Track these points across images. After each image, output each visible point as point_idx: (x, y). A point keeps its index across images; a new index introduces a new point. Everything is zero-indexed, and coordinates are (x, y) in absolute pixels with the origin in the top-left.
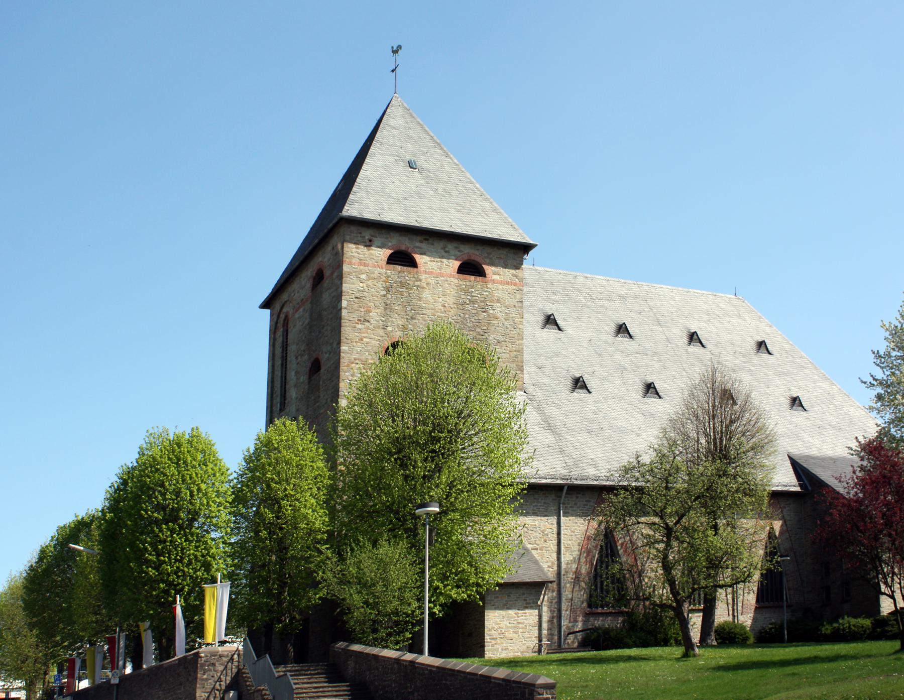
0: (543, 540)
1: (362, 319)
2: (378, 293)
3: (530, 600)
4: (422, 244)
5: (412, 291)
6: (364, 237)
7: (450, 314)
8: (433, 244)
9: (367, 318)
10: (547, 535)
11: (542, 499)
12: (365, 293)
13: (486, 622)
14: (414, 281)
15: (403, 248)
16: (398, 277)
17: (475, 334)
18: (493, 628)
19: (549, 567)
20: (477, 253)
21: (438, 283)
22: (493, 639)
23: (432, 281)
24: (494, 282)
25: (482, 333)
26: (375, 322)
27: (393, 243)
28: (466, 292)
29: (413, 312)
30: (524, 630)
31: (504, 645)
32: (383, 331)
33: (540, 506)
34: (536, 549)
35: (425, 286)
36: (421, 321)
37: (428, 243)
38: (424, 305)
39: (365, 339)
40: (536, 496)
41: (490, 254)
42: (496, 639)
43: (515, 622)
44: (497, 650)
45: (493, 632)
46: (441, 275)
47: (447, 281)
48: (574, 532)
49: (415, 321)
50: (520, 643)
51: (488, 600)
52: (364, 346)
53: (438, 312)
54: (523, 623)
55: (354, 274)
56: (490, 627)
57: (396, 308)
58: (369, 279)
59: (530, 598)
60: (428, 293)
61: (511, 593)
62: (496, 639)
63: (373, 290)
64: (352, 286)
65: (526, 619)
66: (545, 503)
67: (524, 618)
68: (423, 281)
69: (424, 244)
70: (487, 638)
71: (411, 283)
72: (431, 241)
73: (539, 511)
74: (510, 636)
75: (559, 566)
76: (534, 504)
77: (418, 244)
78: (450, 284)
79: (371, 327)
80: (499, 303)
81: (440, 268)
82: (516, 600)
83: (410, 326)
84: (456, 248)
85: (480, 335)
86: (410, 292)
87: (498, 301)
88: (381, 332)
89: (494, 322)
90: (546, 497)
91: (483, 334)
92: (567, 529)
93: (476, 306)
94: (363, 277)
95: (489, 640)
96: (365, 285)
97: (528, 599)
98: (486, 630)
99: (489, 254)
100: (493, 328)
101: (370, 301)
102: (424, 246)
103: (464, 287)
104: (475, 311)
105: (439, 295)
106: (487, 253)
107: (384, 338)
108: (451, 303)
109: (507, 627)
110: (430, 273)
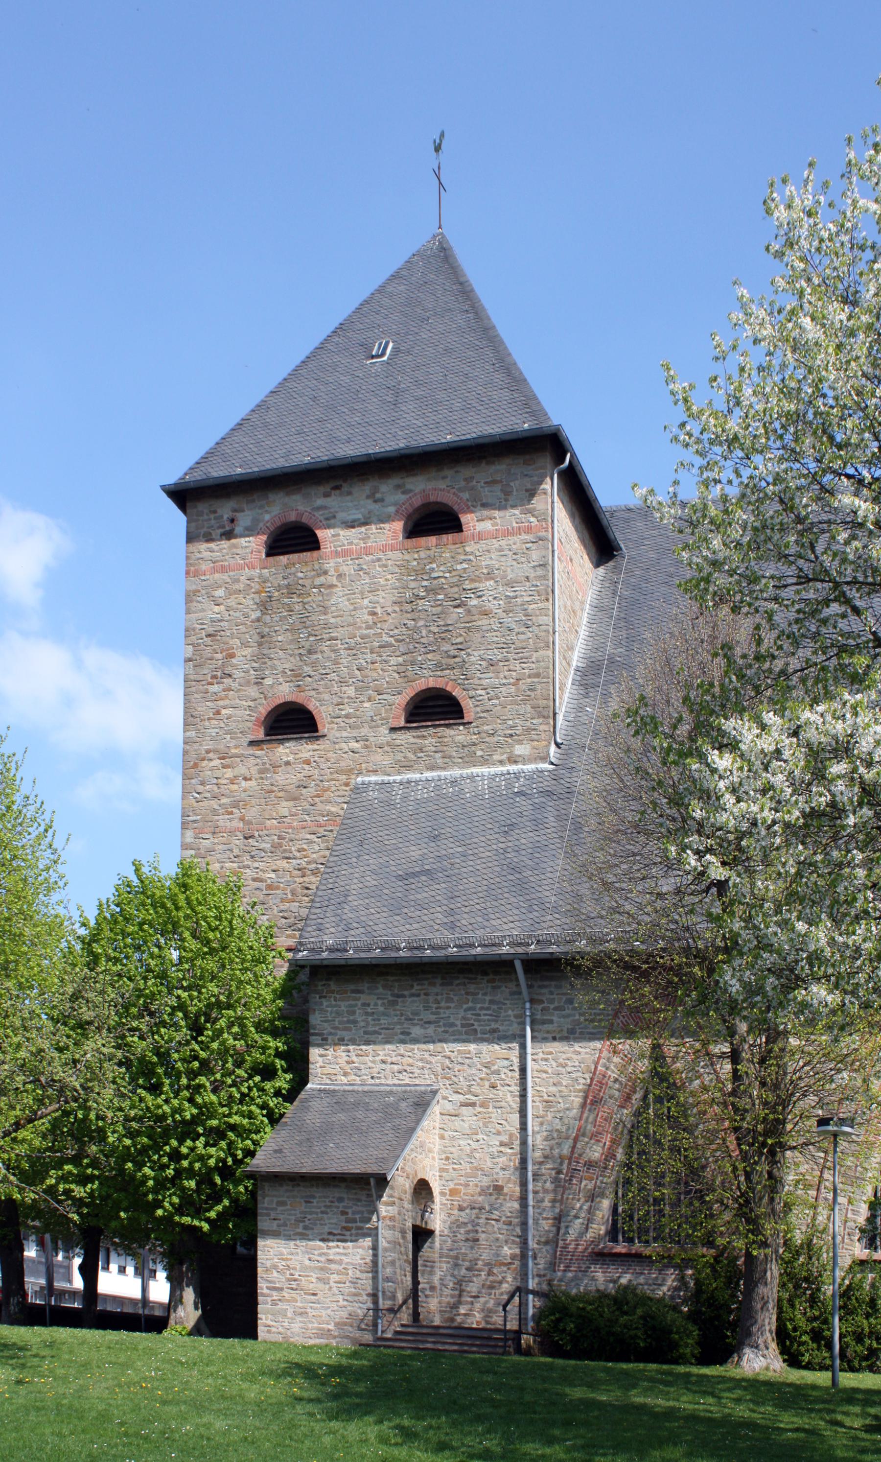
0: (487, 1084)
1: (219, 674)
2: (246, 616)
3: (354, 1213)
4: (329, 499)
5: (310, 599)
6: (222, 517)
7: (385, 626)
8: (350, 493)
9: (228, 670)
10: (497, 1072)
11: (485, 994)
12: (222, 624)
13: (259, 1253)
14: (313, 577)
15: (292, 517)
16: (284, 578)
17: (438, 657)
18: (275, 1267)
19: (502, 1144)
20: (442, 485)
21: (362, 569)
22: (275, 1289)
23: (348, 568)
24: (480, 537)
25: (452, 653)
26: (243, 674)
27: (273, 514)
28: (420, 572)
29: (312, 639)
30: (343, 1278)
31: (299, 1304)
32: (256, 688)
33: (481, 1009)
34: (473, 1105)
35: (335, 582)
36: (328, 653)
37: (341, 495)
38: (332, 620)
39: (224, 712)
40: (472, 988)
41: (472, 478)
42: (282, 1289)
43: (323, 1259)
44: (284, 1313)
45: (275, 1274)
46: (368, 551)
47: (379, 560)
48: (564, 1066)
49: (315, 656)
50: (334, 1305)
51: (263, 1208)
52: (223, 725)
53: (360, 628)
54: (340, 1262)
55: (203, 592)
56: (268, 1264)
57: (280, 639)
58: (230, 593)
59: (355, 1208)
60: (341, 594)
61: (314, 1197)
62: (282, 1289)
63: (237, 614)
64: (201, 615)
65: (345, 1254)
66: (492, 1002)
67: (341, 1251)
68: (332, 572)
69: (333, 497)
70: (262, 1286)
71: (307, 583)
72: (345, 487)
73: (479, 1021)
74: (311, 1286)
75: (524, 1143)
76: (465, 1006)
77: (320, 502)
78: (386, 566)
79: (234, 685)
80: (492, 579)
81: (365, 539)
82: (322, 1212)
83: (306, 668)
84: (398, 487)
85: (449, 657)
86: (306, 600)
87: (489, 576)
88: (253, 691)
89: (480, 623)
90: (494, 988)
91: (455, 653)
92: (546, 1060)
93: (441, 597)
94: (220, 593)
95: (265, 1291)
96: (222, 608)
97: (350, 1211)
98: (259, 1270)
99: (468, 480)
100: (476, 637)
101: (232, 636)
102: (333, 502)
103: (415, 563)
104: (439, 609)
105: (362, 593)
106: (465, 480)
107: (258, 701)
108: (389, 603)
109: (304, 1268)
110: (346, 553)
